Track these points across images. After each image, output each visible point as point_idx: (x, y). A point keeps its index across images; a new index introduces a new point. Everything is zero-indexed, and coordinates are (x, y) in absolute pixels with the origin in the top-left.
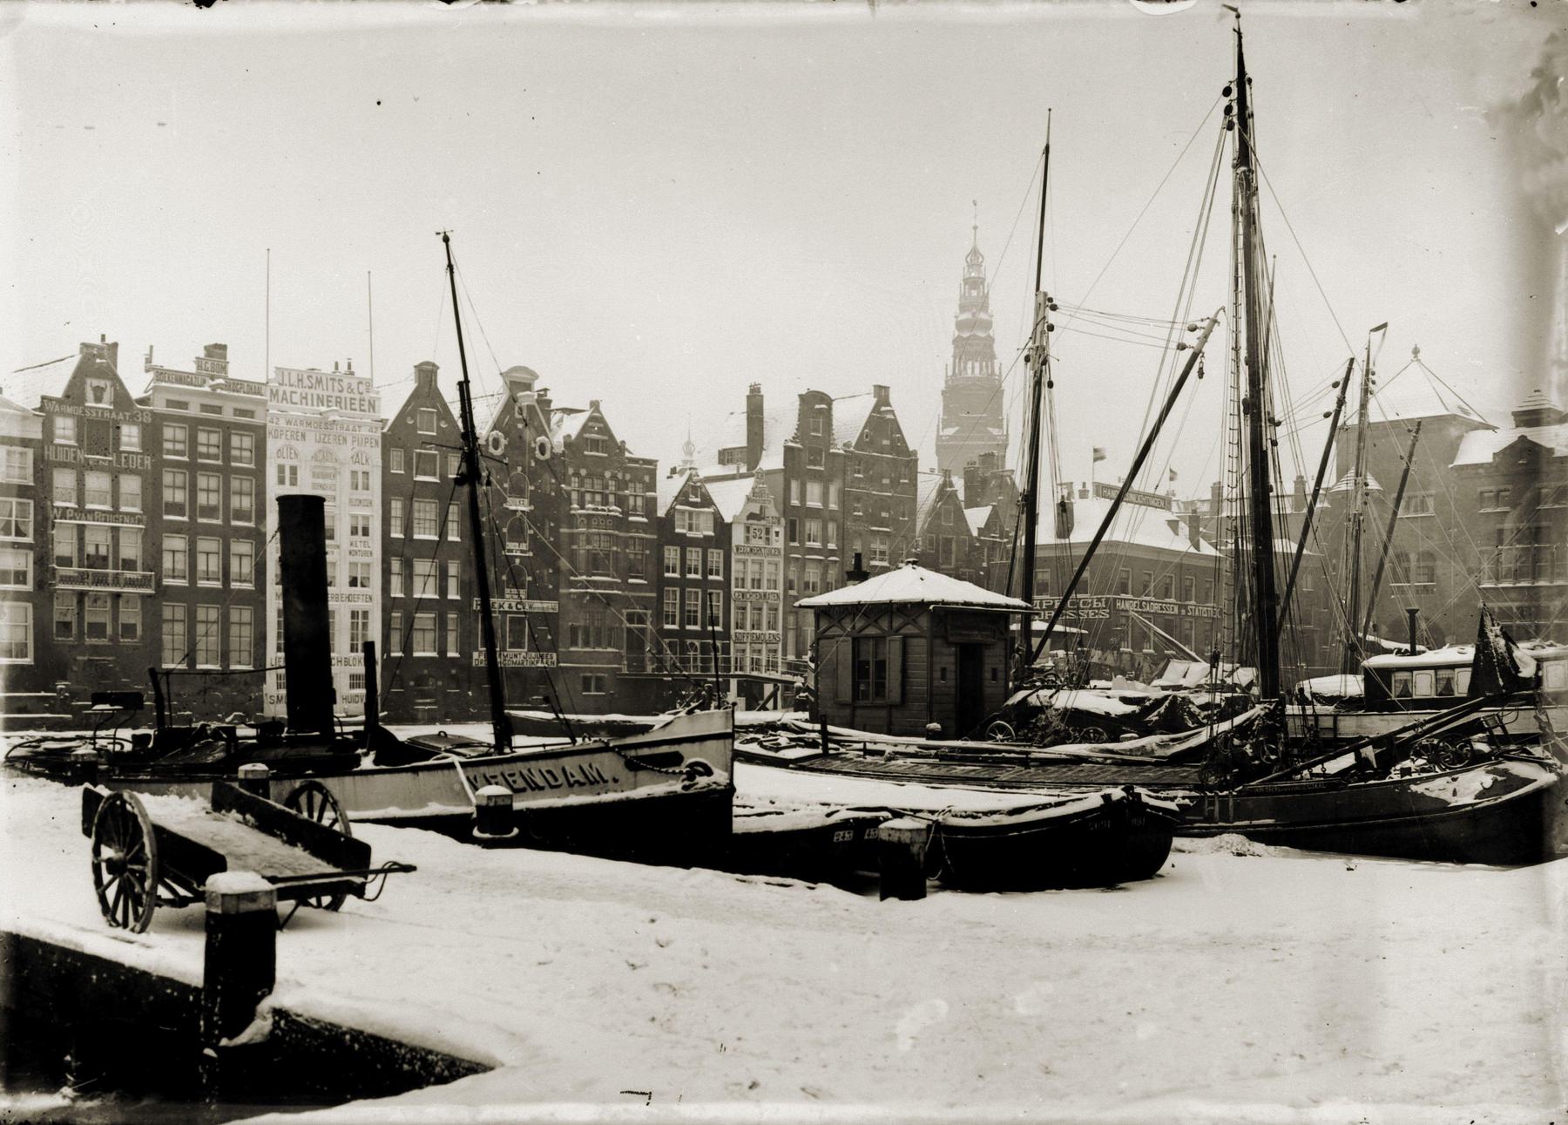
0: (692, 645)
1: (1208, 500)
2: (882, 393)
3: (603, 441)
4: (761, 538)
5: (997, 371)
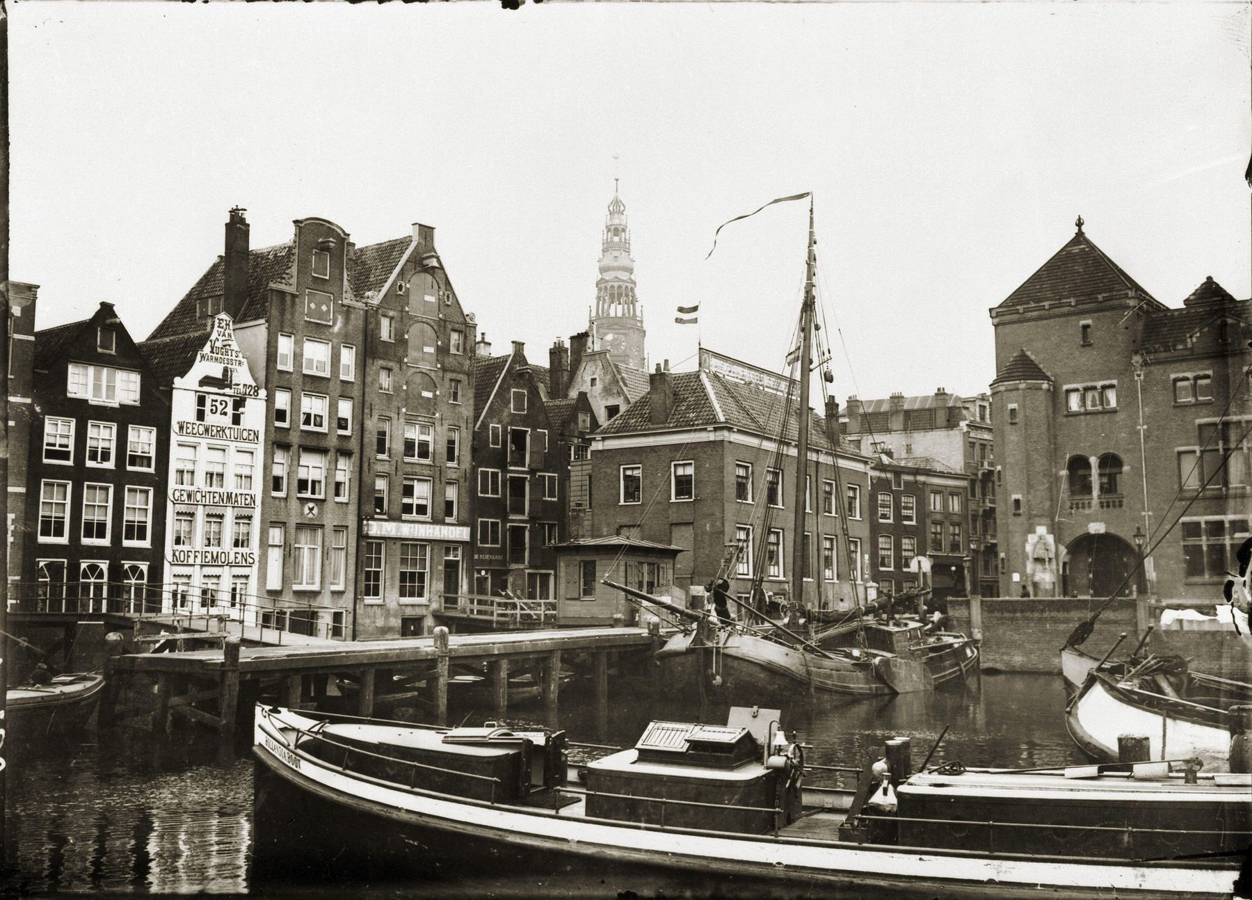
0: (134, 569)
4: (225, 414)
5: (638, 313)
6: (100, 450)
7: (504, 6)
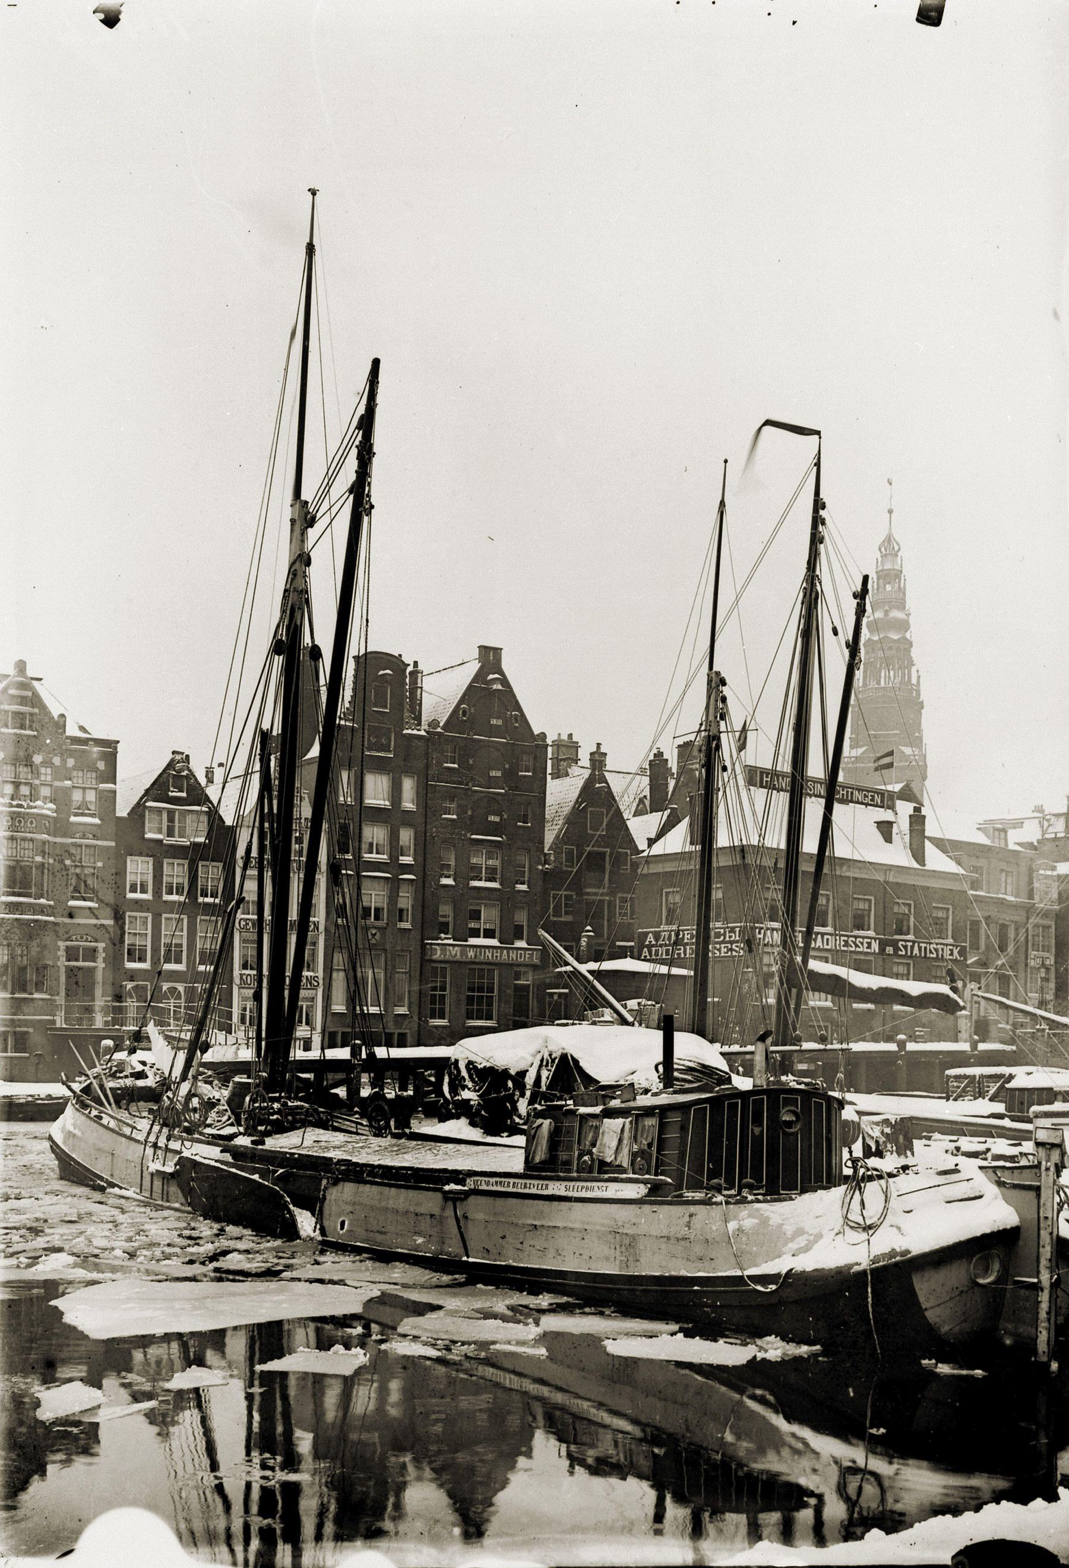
0: (173, 990)
1: (1064, 814)
2: (490, 657)
3: (31, 714)
6: (175, 885)
7: (1059, 1499)
